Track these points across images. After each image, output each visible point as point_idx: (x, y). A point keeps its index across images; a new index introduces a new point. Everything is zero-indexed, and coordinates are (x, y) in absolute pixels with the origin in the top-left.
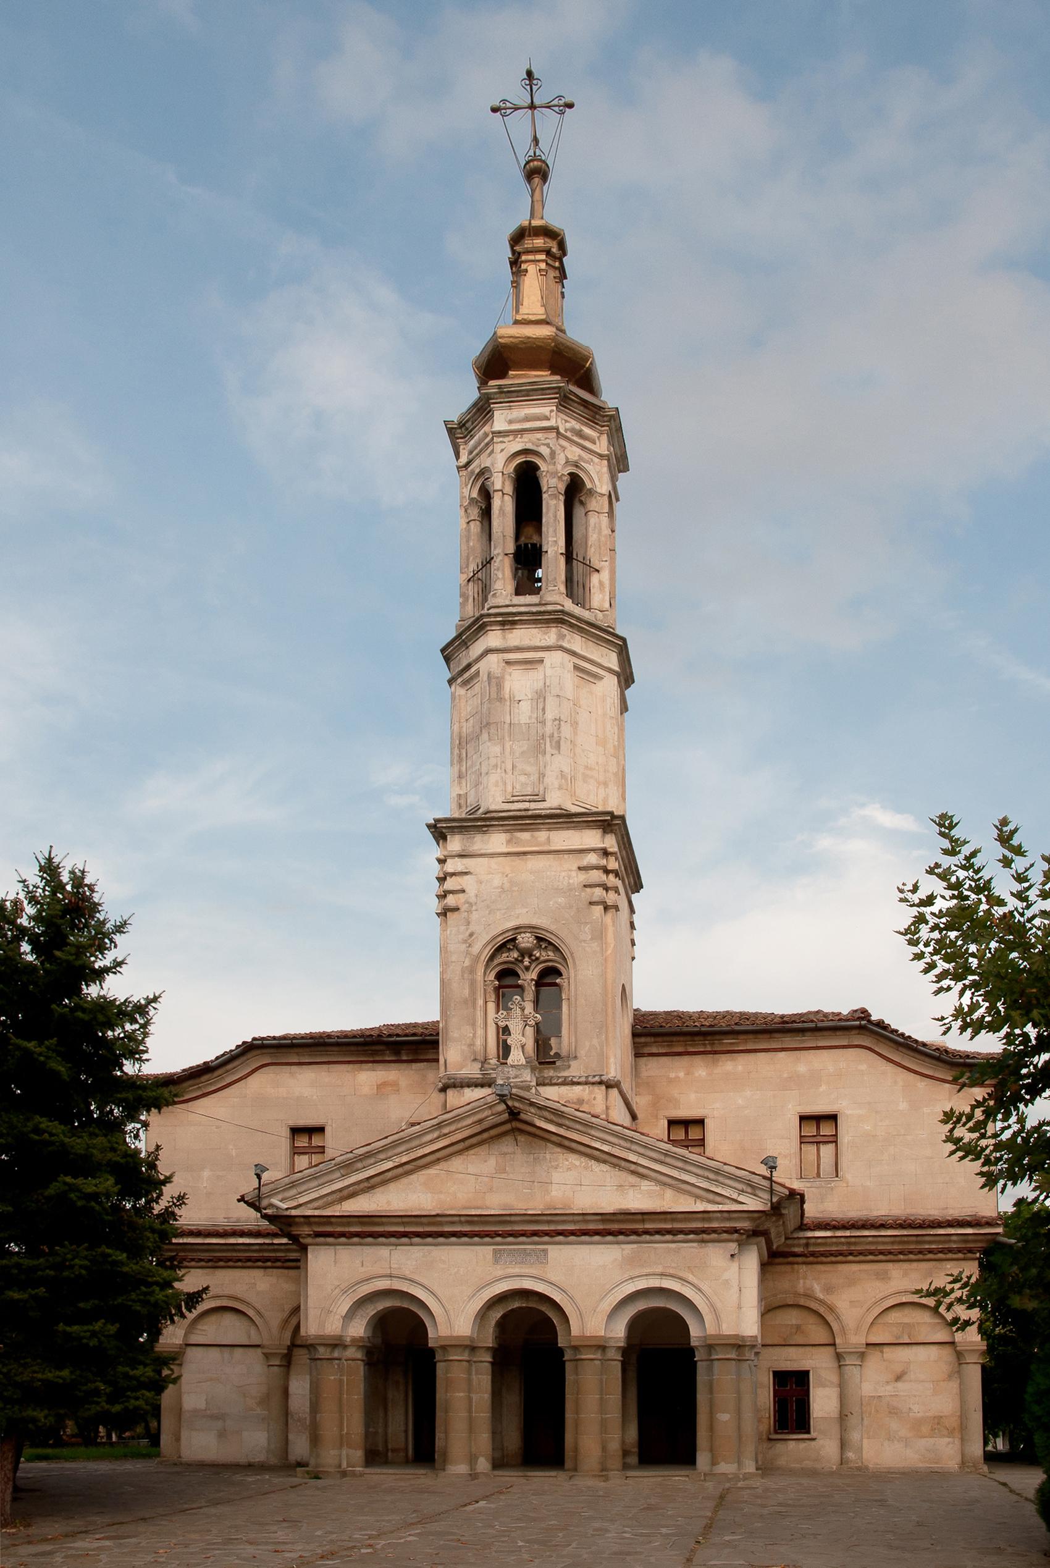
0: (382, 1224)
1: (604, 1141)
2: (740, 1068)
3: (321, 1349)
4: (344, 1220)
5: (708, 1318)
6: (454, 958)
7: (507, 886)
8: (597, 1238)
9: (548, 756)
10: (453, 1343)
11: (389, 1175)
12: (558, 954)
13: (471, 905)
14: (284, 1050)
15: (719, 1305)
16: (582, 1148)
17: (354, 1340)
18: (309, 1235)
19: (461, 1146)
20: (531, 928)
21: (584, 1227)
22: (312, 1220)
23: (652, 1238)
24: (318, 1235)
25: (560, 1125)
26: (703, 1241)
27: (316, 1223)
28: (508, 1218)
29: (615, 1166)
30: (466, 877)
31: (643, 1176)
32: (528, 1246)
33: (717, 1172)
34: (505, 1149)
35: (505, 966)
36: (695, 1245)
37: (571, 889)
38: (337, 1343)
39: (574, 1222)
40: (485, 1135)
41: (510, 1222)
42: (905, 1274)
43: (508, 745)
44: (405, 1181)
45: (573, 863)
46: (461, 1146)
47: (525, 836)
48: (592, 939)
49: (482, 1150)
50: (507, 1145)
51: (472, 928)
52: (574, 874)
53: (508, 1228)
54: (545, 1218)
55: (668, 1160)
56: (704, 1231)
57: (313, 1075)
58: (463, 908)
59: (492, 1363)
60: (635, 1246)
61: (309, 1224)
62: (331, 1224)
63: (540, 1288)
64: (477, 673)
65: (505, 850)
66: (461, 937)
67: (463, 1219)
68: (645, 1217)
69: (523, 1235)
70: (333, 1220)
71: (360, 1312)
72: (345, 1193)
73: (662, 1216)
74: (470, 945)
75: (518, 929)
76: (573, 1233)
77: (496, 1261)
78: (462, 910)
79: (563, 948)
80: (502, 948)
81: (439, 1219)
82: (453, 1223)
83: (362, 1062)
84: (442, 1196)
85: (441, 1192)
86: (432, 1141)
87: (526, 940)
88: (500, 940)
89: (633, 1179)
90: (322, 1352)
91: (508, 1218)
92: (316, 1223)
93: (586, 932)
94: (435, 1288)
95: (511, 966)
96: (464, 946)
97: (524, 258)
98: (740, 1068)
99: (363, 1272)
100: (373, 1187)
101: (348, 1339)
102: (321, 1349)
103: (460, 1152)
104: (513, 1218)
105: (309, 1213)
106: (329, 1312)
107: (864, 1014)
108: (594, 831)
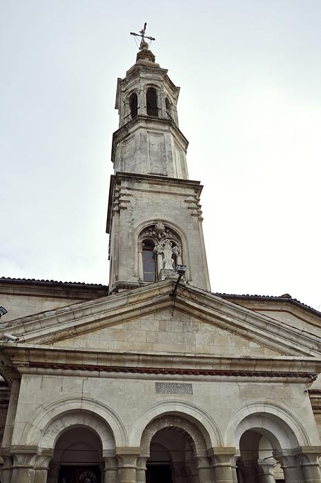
0: (82, 359)
1: (228, 315)
3: (20, 459)
4: (56, 354)
5: (298, 434)
6: (124, 228)
8: (224, 377)
9: (167, 162)
10: (128, 452)
11: (90, 326)
13: (133, 208)
14: (7, 285)
15: (304, 425)
16: (214, 320)
17: (45, 452)
18: (26, 365)
19: (138, 312)
21: (217, 368)
22: (32, 352)
23: (258, 378)
24: (32, 365)
25: (201, 304)
26: (286, 382)
27: (33, 355)
28: (171, 359)
29: (232, 331)
31: (250, 339)
32: (178, 379)
33: (298, 336)
36: (282, 384)
37: (181, 208)
38: (31, 452)
39: (213, 364)
41: (172, 362)
43: (123, 191)
44: (99, 332)
45: (183, 199)
46: (138, 312)
50: (166, 316)
51: (133, 217)
53: (169, 367)
54: (195, 360)
55: (268, 328)
56: (289, 375)
57: (20, 301)
59: (146, 471)
60: (246, 384)
61: (28, 356)
62: (45, 356)
63: (188, 411)
64: (134, 136)
67: (141, 358)
68: (258, 362)
69: (177, 373)
70: (47, 353)
71: (52, 428)
72: (58, 336)
73: (268, 363)
76: (210, 373)
77: (158, 391)
79: (180, 234)
81: (124, 357)
82: (133, 361)
83: (47, 297)
84: (124, 344)
85: (123, 341)
87: (161, 226)
88: (147, 225)
89: (243, 340)
90: (20, 461)
91: (171, 359)
92: (33, 355)
93: (191, 226)
94: (115, 410)
99: (67, 393)
100: (77, 334)
101: (40, 450)
102: (20, 459)
104: (175, 359)
105: (31, 346)
106: (32, 425)
107: (288, 296)
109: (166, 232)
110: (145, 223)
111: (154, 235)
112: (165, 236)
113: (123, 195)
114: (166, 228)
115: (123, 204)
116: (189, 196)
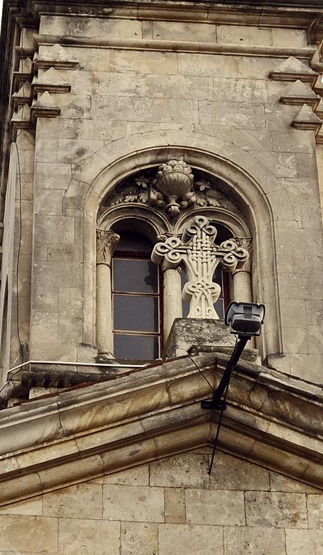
2: (296, 414)
6: (48, 184)
7: (144, 90)
12: (227, 204)
13: (81, 110)
20: (188, 153)
30: (76, 72)
34: (181, 478)
35: (129, 216)
37: (256, 103)
40: (146, 447)
42: (24, 460)
45: (261, 68)
47: (177, 27)
48: (298, 176)
49: (136, 478)
50: (187, 473)
51: (81, 143)
52: (260, 84)
58: (66, 114)
65: (139, 40)
66: (61, 154)
74: (78, 167)
75: (163, 152)
78: (65, 114)
80: (127, 185)
86: (39, 445)
87: (179, 171)
88: (129, 167)
95: (140, 216)
96: (68, 167)
97: (43, 78)
98: (296, 414)
103: (88, 477)
108: (292, 32)
109: (196, 190)
110: (121, 161)
111: (153, 204)
112: (191, 205)
113: (48, 65)
114: (199, 176)
115: (45, 100)
116: (284, 55)
